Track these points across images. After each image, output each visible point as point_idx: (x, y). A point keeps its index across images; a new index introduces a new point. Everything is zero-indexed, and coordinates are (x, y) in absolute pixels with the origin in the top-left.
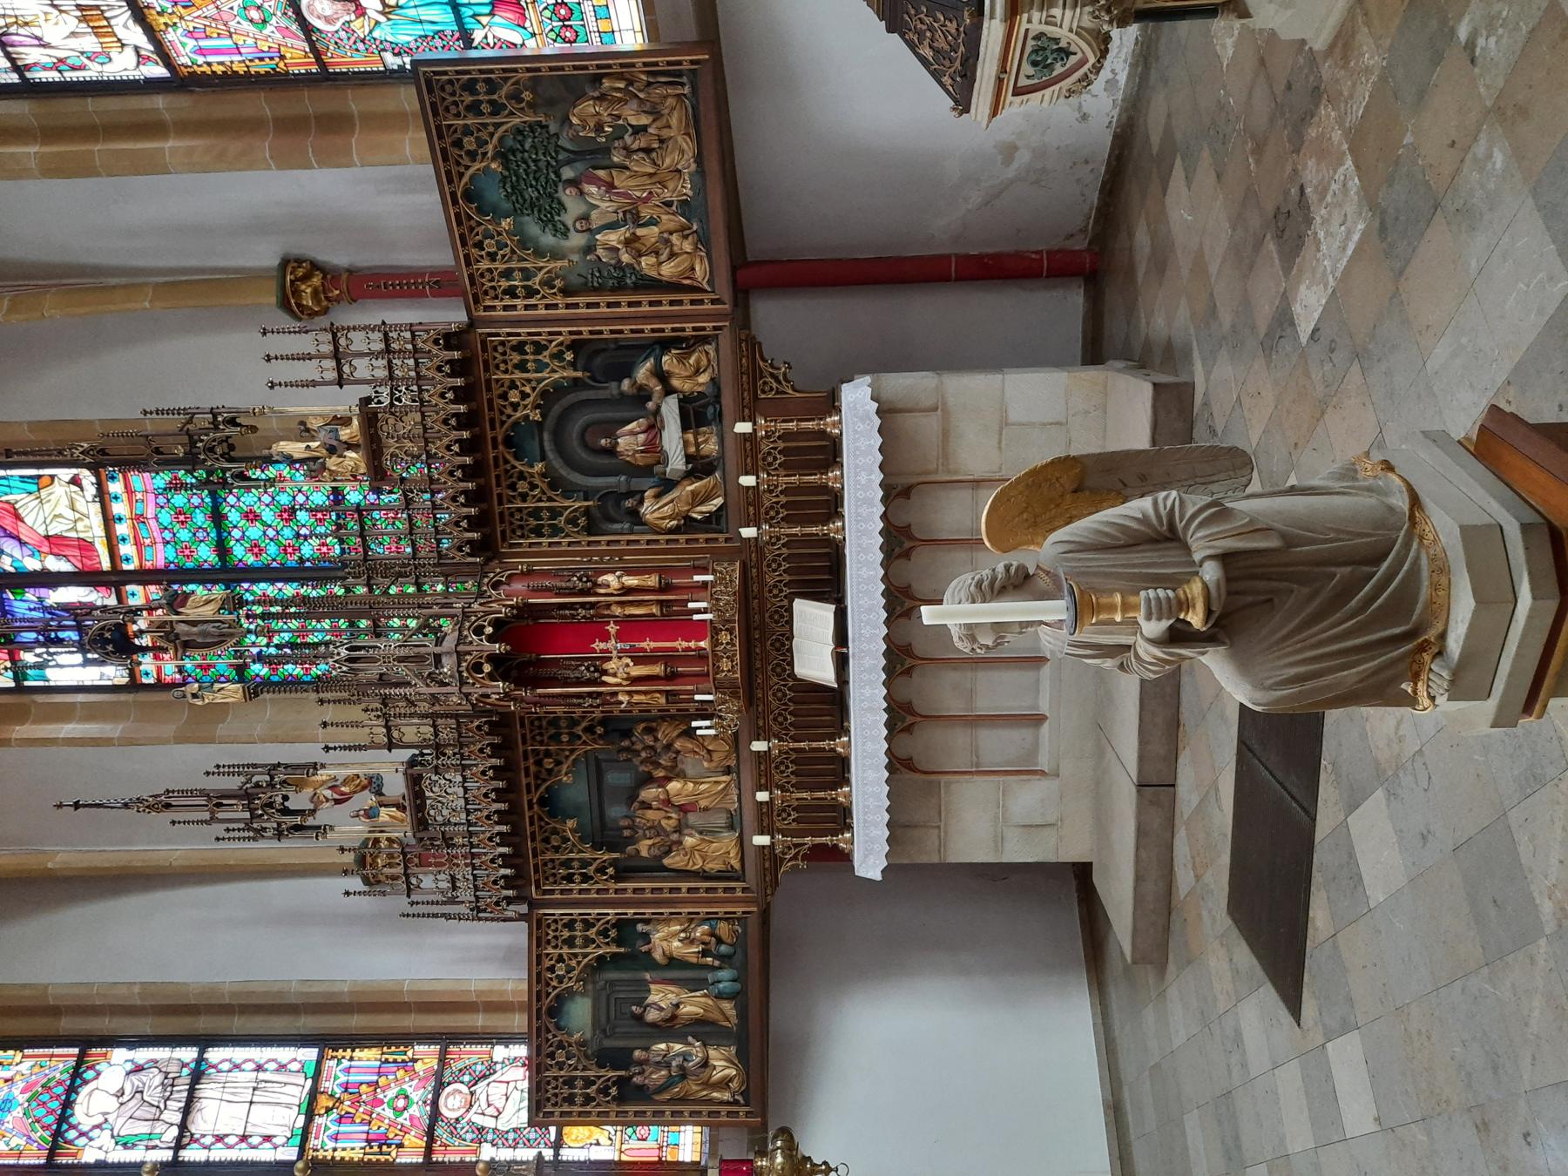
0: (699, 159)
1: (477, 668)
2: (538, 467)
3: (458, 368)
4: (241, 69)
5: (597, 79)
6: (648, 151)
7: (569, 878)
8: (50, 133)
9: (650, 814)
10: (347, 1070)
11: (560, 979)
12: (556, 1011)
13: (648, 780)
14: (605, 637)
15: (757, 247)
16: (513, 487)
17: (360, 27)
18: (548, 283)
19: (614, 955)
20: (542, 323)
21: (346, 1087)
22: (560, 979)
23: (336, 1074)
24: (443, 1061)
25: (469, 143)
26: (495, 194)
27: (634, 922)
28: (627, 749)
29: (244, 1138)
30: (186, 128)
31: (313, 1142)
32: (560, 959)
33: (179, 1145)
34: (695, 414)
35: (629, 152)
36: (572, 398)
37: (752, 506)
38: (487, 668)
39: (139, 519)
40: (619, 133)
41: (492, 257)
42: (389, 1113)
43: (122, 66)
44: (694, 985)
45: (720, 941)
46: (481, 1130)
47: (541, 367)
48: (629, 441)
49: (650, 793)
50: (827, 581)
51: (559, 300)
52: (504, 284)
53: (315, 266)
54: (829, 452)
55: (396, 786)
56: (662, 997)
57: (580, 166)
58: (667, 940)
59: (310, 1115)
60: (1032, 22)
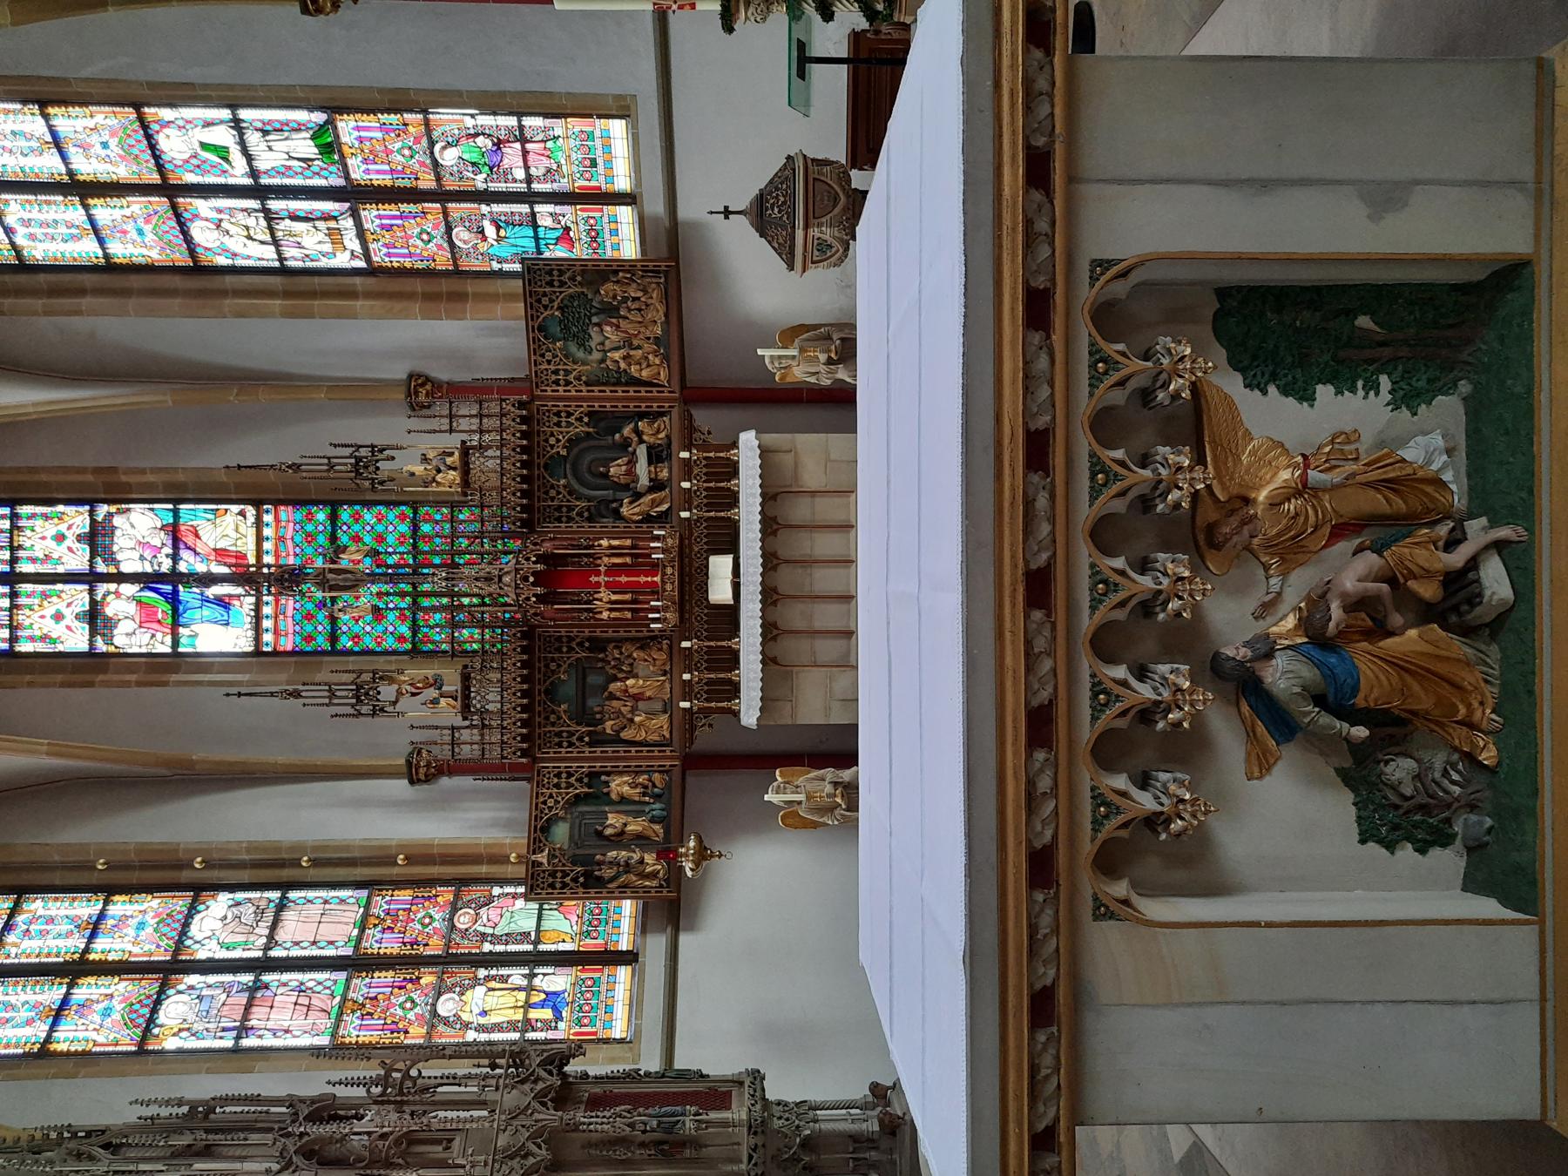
0: (666, 315)
1: (525, 579)
2: (563, 482)
3: (524, 420)
4: (408, 265)
5: (616, 272)
6: (640, 310)
7: (560, 745)
8: (287, 294)
9: (615, 703)
10: (388, 903)
11: (550, 808)
12: (546, 829)
13: (615, 679)
14: (598, 574)
15: (693, 378)
16: (547, 493)
17: (483, 247)
18: (578, 378)
19: (587, 794)
20: (572, 401)
21: (388, 913)
22: (550, 808)
23: (380, 904)
24: (457, 896)
25: (545, 301)
26: (556, 329)
27: (599, 774)
28: (602, 660)
29: (314, 943)
30: (368, 295)
31: (364, 944)
32: (551, 796)
33: (267, 948)
34: (655, 456)
35: (630, 310)
36: (584, 445)
37: (687, 499)
38: (531, 579)
39: (281, 539)
40: (625, 300)
41: (549, 362)
42: (419, 927)
43: (342, 260)
44: (637, 814)
45: (654, 786)
46: (484, 934)
47: (569, 424)
48: (616, 470)
49: (615, 687)
50: (728, 543)
51: (584, 388)
52: (554, 377)
53: (428, 379)
54: (732, 470)
55: (453, 684)
56: (614, 820)
57: (602, 316)
58: (619, 786)
59: (362, 930)
60: (814, 232)
